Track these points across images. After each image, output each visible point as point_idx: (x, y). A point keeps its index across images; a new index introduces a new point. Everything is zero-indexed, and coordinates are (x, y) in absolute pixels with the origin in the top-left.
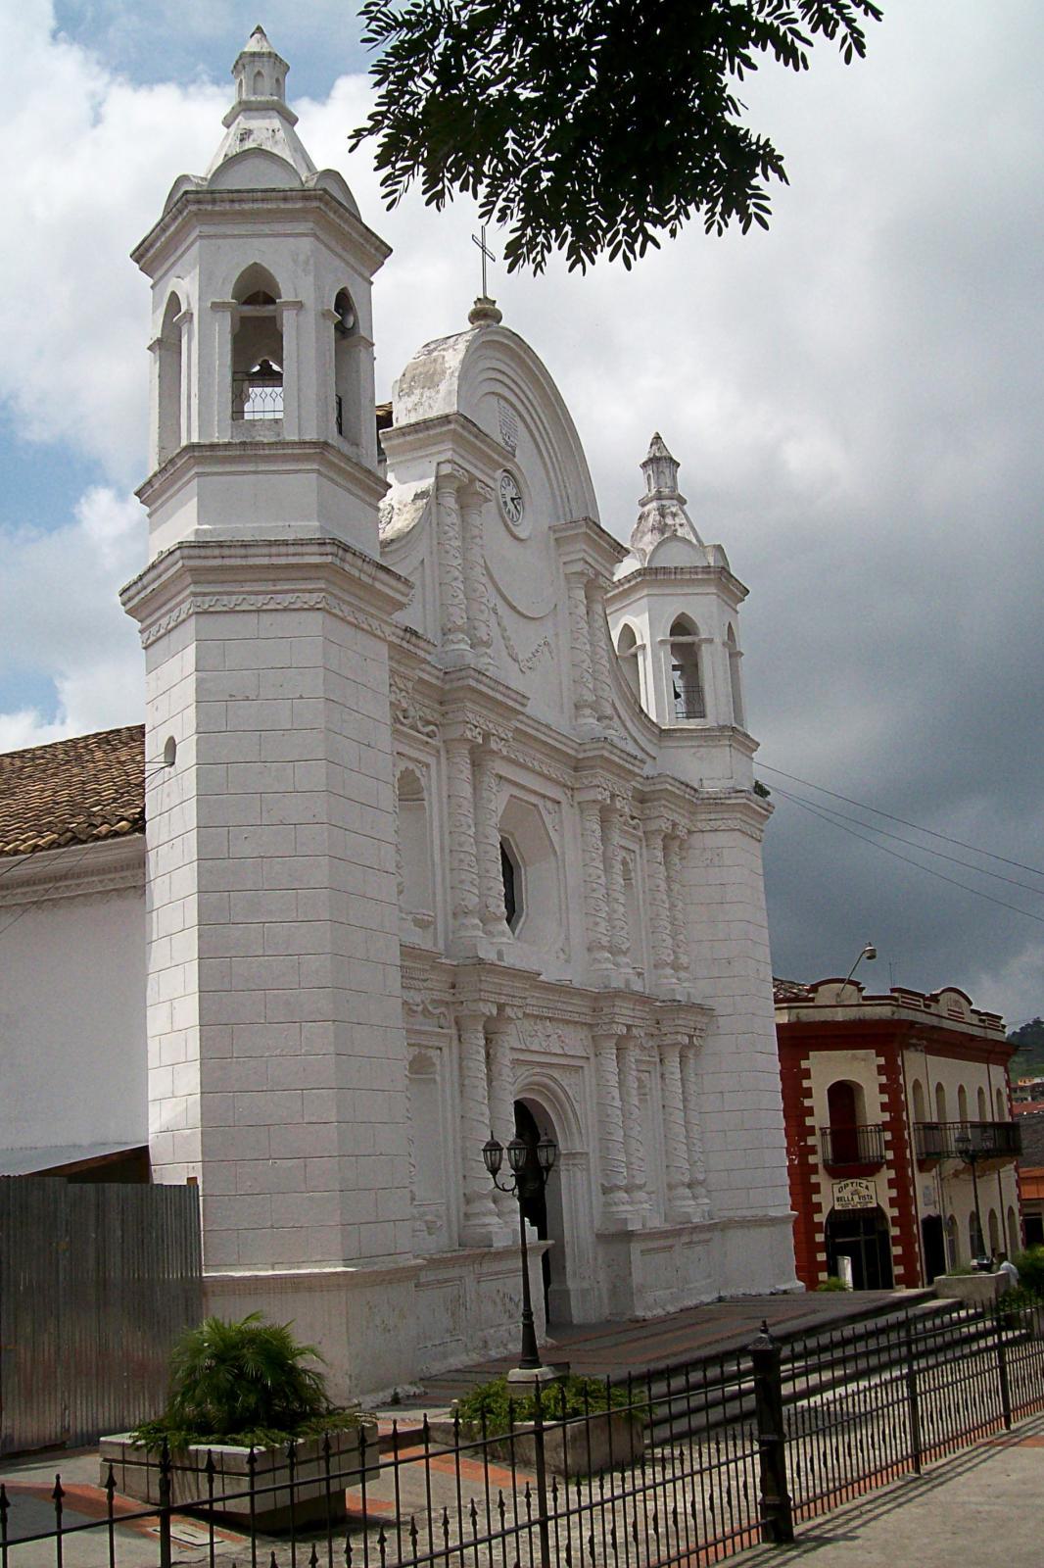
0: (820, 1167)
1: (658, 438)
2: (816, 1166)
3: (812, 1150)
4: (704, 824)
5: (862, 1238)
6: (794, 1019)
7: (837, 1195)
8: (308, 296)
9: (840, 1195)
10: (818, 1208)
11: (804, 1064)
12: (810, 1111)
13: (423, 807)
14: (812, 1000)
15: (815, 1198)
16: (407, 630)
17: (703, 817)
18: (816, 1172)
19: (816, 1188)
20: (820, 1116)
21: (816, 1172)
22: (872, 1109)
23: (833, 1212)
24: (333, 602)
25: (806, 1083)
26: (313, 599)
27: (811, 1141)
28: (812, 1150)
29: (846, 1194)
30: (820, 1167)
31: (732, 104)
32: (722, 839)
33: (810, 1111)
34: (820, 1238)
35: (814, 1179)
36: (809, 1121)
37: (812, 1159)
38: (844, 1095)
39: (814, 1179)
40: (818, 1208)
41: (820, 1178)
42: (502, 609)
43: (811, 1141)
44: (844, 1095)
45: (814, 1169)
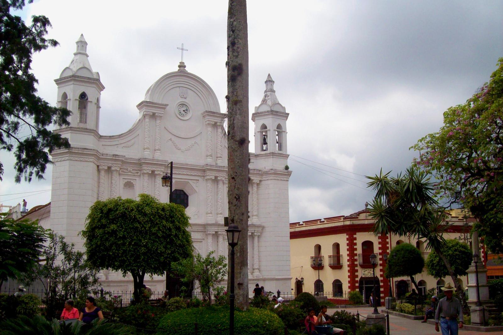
0: (358, 265)
1: (269, 75)
2: (357, 264)
3: (356, 260)
4: (265, 178)
5: (364, 286)
6: (351, 223)
7: (363, 273)
8: (71, 98)
9: (364, 273)
10: (357, 276)
11: (355, 236)
12: (356, 249)
13: (134, 189)
14: (358, 218)
15: (356, 274)
16: (113, 155)
17: (264, 176)
18: (357, 266)
19: (357, 271)
20: (359, 250)
21: (357, 266)
22: (377, 249)
23: (362, 278)
24: (70, 157)
25: (355, 241)
26: (67, 158)
27: (356, 258)
28: (356, 260)
29: (366, 273)
30: (358, 265)
31: (35, 90)
32: (269, 182)
33: (356, 249)
34: (357, 285)
35: (356, 268)
36: (355, 252)
37: (356, 263)
38: (368, 245)
39: (356, 268)
40: (357, 276)
41: (358, 268)
42: (174, 139)
43: (356, 258)
44: (368, 245)
45: (356, 265)
